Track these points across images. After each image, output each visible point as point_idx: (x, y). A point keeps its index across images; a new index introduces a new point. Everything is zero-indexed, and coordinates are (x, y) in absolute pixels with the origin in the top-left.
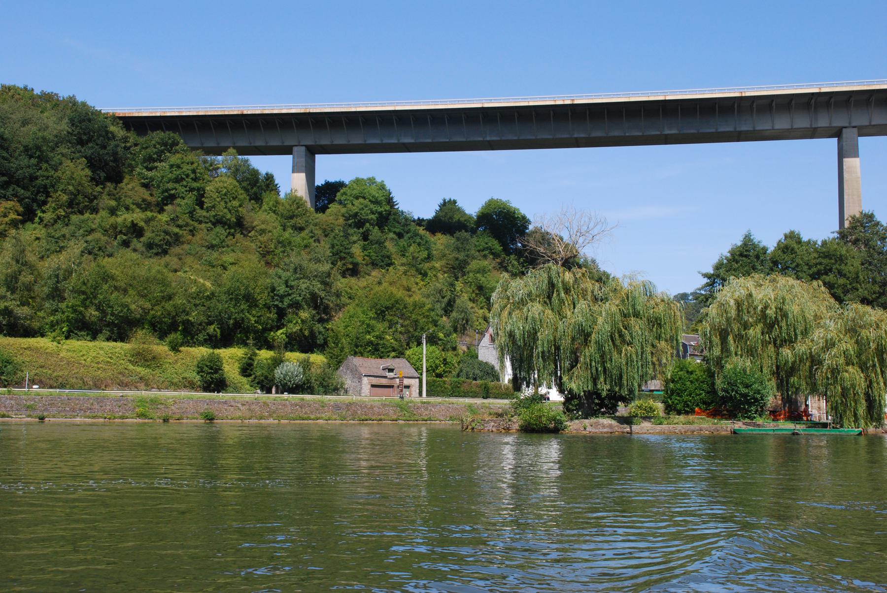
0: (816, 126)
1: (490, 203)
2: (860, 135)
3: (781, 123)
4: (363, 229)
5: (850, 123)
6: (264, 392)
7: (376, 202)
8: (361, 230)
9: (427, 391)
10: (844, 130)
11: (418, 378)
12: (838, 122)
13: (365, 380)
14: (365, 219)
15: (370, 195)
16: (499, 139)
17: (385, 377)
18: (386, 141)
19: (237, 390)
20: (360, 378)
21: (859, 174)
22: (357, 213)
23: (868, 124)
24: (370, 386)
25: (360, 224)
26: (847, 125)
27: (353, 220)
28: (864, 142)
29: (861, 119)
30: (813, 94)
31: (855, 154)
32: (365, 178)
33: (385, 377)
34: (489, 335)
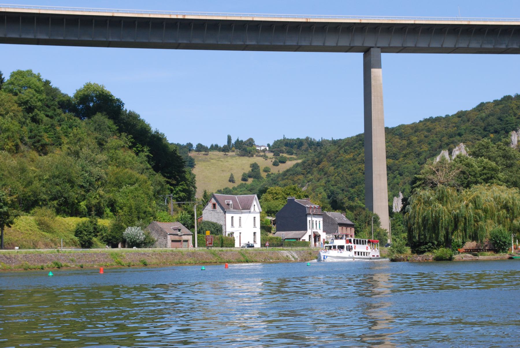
0: (353, 45)
1: (88, 86)
2: (383, 52)
3: (331, 42)
4: (32, 113)
5: (376, 45)
6: (110, 247)
7: (38, 91)
8: (31, 115)
9: (198, 243)
10: (372, 49)
11: (192, 235)
12: (368, 44)
13: (169, 237)
14: (34, 106)
15: (35, 85)
16: (119, 40)
17: (177, 235)
18: (24, 36)
19: (97, 247)
20: (166, 236)
21: (381, 82)
22: (28, 101)
23: (387, 46)
24: (171, 241)
25: (30, 110)
26: (374, 45)
27: (25, 107)
28: (385, 57)
29: (383, 42)
30: (355, 23)
31: (379, 66)
32: (25, 70)
33: (177, 235)
34: (211, 204)
